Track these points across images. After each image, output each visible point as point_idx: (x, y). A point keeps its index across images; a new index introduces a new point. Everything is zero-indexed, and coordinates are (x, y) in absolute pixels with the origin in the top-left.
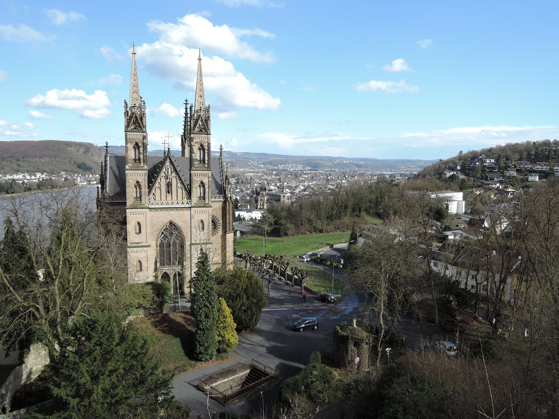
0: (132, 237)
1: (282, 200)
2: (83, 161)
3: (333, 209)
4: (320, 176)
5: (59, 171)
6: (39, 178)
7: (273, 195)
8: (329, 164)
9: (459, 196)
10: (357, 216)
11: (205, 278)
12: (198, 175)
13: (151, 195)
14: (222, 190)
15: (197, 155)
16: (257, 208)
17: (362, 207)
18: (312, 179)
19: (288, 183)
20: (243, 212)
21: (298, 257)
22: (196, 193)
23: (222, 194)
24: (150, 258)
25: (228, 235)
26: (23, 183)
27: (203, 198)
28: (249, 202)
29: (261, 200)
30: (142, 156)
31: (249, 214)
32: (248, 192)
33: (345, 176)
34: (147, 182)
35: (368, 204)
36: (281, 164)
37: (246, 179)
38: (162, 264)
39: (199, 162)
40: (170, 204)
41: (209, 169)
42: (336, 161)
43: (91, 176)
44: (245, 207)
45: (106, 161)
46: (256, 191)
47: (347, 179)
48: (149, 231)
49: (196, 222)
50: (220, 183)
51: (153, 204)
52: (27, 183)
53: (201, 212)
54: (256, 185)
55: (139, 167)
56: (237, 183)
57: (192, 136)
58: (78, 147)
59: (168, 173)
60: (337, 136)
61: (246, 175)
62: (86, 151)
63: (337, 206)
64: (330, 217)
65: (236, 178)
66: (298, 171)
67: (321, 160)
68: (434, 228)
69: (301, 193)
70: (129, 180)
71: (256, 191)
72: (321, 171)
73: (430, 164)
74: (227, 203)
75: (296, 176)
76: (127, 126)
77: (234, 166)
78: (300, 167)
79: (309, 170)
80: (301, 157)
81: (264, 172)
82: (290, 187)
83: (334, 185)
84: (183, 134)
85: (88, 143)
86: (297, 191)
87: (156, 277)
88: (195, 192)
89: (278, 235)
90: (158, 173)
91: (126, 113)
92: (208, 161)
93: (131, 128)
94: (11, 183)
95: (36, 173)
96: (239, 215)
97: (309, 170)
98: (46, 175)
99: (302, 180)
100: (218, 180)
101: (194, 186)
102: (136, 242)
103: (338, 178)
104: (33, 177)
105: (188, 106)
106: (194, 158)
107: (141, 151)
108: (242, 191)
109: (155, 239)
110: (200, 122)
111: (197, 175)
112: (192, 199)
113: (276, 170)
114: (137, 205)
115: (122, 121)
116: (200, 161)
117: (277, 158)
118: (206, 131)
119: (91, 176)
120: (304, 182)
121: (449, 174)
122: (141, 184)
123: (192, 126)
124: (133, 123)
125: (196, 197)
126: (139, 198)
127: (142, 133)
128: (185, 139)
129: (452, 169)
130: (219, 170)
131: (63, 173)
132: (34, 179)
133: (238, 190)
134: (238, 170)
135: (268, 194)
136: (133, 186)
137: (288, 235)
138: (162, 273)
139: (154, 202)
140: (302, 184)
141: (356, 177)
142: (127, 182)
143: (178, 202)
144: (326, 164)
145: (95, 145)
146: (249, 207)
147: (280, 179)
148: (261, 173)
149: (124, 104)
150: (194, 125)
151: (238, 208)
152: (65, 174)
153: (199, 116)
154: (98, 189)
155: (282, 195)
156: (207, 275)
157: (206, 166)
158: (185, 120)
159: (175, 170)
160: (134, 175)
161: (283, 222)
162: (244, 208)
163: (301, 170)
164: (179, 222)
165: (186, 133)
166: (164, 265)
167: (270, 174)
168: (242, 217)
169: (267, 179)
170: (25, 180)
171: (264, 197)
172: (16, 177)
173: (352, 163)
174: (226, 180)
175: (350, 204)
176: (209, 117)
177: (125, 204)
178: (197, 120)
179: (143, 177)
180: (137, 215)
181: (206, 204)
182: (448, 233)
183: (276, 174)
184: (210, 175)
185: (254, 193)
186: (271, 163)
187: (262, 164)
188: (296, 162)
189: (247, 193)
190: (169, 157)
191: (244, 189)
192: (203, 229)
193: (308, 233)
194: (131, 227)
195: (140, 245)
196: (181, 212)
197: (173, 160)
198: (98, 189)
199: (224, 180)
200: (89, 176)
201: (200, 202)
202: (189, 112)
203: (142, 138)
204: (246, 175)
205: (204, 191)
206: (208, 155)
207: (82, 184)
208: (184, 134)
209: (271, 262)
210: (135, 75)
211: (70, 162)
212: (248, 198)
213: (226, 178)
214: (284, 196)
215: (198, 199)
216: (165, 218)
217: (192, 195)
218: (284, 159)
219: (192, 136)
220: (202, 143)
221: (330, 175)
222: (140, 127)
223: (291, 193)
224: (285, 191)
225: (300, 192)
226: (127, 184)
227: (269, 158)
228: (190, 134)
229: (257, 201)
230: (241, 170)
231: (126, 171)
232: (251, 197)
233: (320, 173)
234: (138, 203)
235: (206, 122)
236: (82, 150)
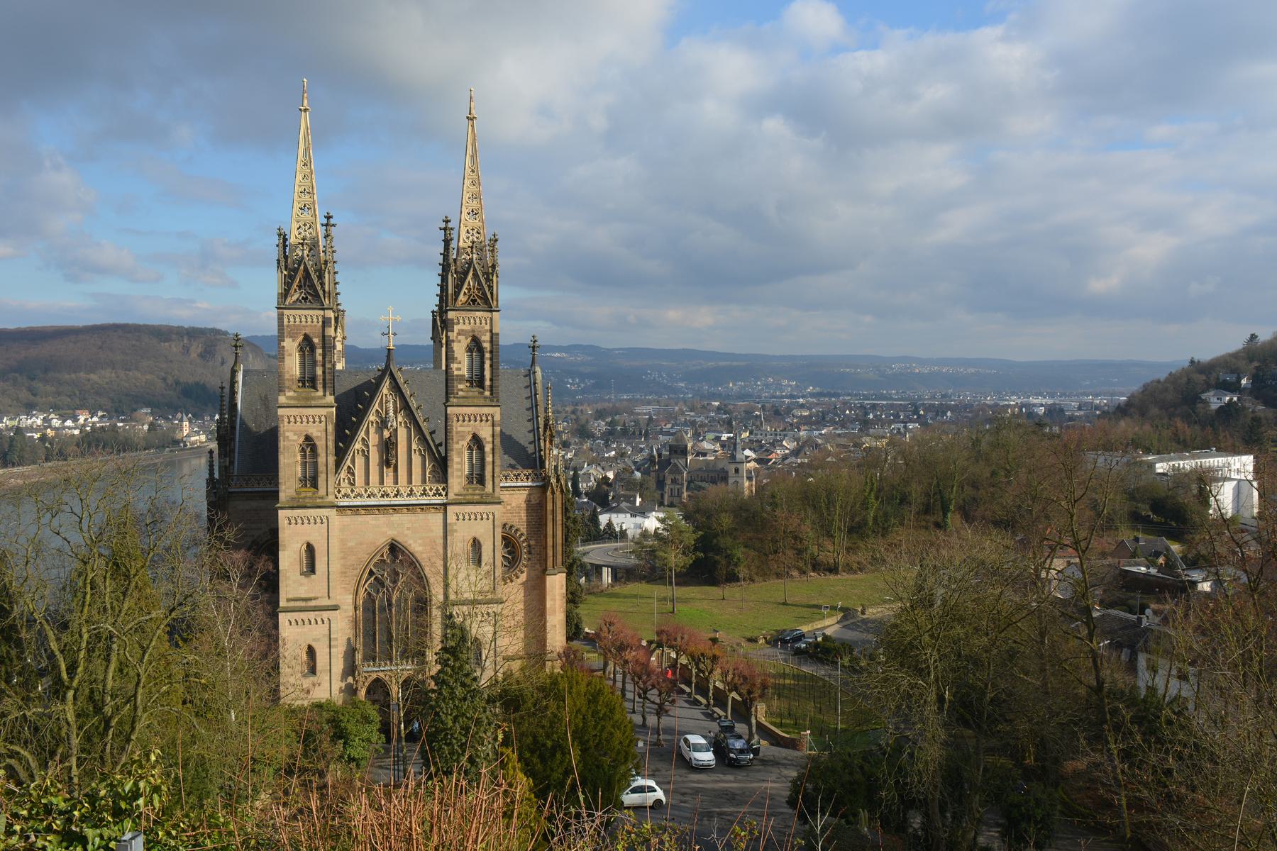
0: (292, 584)
1: (731, 481)
5: (135, 406)
6: (84, 426)
9: (1243, 464)
10: (938, 526)
11: (459, 692)
12: (466, 418)
13: (343, 474)
15: (462, 366)
19: (751, 433)
20: (621, 516)
21: (762, 641)
22: (459, 466)
24: (336, 639)
25: (549, 579)
26: (43, 438)
27: (477, 477)
28: (641, 487)
30: (319, 371)
31: (639, 520)
33: (916, 412)
34: (331, 438)
35: (968, 490)
37: (637, 422)
38: (370, 657)
39: (468, 384)
40: (392, 495)
41: (494, 400)
45: (233, 382)
48: (336, 567)
49: (459, 543)
51: (346, 495)
52: (53, 438)
53: (473, 517)
55: (314, 398)
57: (451, 315)
59: (387, 413)
63: (877, 498)
64: (857, 530)
65: (609, 420)
66: (782, 397)
68: (1161, 560)
69: (787, 461)
70: (287, 434)
73: (1162, 376)
74: (549, 493)
76: (284, 295)
78: (788, 385)
82: (751, 444)
83: (883, 437)
84: (436, 309)
87: (351, 691)
88: (458, 463)
89: (713, 582)
90: (362, 415)
91: (283, 260)
92: (491, 380)
93: (295, 298)
94: (12, 439)
95: (78, 412)
96: (610, 524)
97: (812, 395)
98: (103, 417)
99: (792, 425)
101: (456, 446)
102: (303, 596)
103: (897, 416)
104: (69, 423)
106: (456, 373)
107: (319, 358)
109: (352, 589)
111: (462, 418)
112: (450, 481)
114: (305, 498)
115: (272, 282)
116: (471, 381)
120: (799, 430)
121: (1216, 401)
122: (318, 443)
124: (300, 287)
125: (459, 477)
126: (311, 480)
127: (321, 312)
129: (1233, 387)
132: (70, 428)
136: (297, 448)
137: (738, 580)
138: (370, 680)
139: (349, 490)
141: (949, 414)
142: (281, 438)
143: (411, 490)
146: (639, 500)
147: (729, 423)
149: (276, 240)
152: (152, 414)
154: (211, 457)
156: (463, 685)
157: (487, 393)
159: (406, 407)
160: (298, 420)
161: (725, 542)
162: (624, 505)
164: (416, 546)
166: (374, 660)
168: (618, 529)
170: (49, 431)
172: (25, 421)
174: (545, 431)
175: (916, 491)
177: (275, 495)
179: (323, 424)
180: (306, 525)
181: (488, 495)
182: (1196, 575)
183: (719, 408)
187: (682, 380)
190: (391, 372)
192: (478, 562)
193: (795, 573)
194: (289, 558)
195: (313, 603)
196: (420, 517)
197: (401, 380)
198: (211, 457)
199: (541, 430)
201: (470, 491)
203: (321, 323)
206: (491, 366)
209: (673, 655)
210: (305, 165)
213: (546, 425)
214: (737, 471)
215: (465, 482)
216: (379, 530)
217: (450, 470)
220: (476, 334)
222: (317, 295)
224: (739, 457)
225: (785, 457)
226: (282, 444)
229: (661, 484)
231: (281, 412)
234: (308, 491)
236: (196, 348)
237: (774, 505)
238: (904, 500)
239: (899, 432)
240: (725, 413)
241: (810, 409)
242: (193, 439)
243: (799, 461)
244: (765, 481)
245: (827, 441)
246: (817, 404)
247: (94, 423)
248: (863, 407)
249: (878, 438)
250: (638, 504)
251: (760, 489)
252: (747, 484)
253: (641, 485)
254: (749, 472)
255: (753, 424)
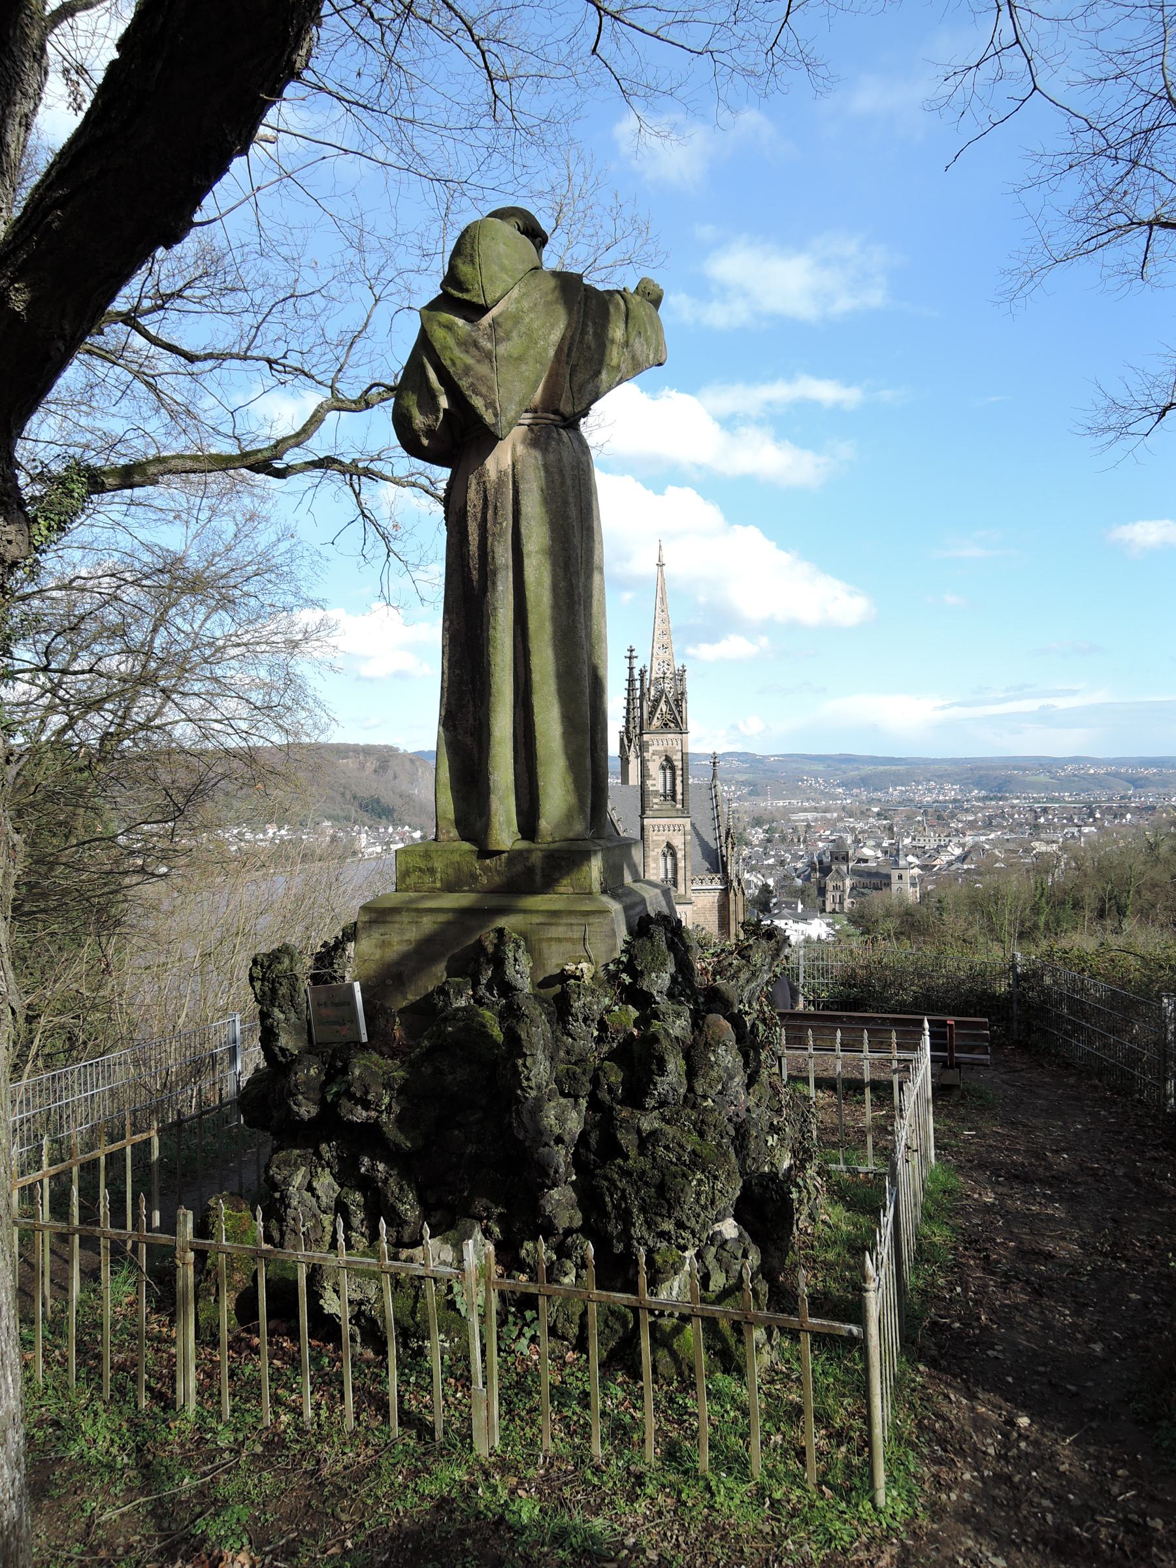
1: (894, 887)
2: (373, 793)
3: (1036, 910)
4: (1012, 816)
5: (317, 819)
7: (870, 874)
8: (1043, 778)
14: (717, 863)
15: (657, 782)
16: (823, 910)
17: (1127, 906)
18: (989, 825)
19: (914, 839)
23: (718, 872)
28: (802, 893)
29: (836, 888)
31: (801, 926)
32: (799, 865)
33: (1091, 814)
36: (895, 785)
37: (795, 829)
41: (685, 812)
42: (1065, 770)
43: (391, 830)
44: (790, 908)
46: (821, 862)
47: (1099, 823)
50: (713, 844)
54: (821, 845)
56: (769, 841)
58: (361, 757)
60: (1074, 692)
61: (794, 817)
62: (380, 767)
63: (1048, 903)
65: (766, 827)
66: (946, 801)
67: (1015, 769)
69: (953, 867)
71: (821, 862)
72: (1016, 802)
74: (732, 895)
75: (940, 817)
77: (758, 795)
78: (952, 792)
79: (978, 799)
80: (955, 761)
81: (844, 808)
84: (623, 729)
85: (386, 746)
86: (943, 859)
97: (978, 799)
99: (956, 830)
100: (709, 837)
101: (652, 853)
103: (1070, 819)
105: (636, 673)
106: (651, 788)
108: (782, 863)
110: (663, 706)
113: (879, 800)
117: (881, 768)
118: (677, 725)
119: (391, 830)
123: (645, 716)
128: (630, 741)
130: (710, 814)
131: (327, 823)
132: (261, 840)
133: (771, 861)
134: (771, 804)
135: (855, 872)
140: (955, 840)
141: (1129, 816)
144: (1034, 778)
145: (401, 751)
146: (800, 907)
147: (891, 828)
148: (835, 810)
150: (650, 713)
151: (769, 911)
153: (662, 692)
155: (895, 874)
157: (679, 806)
158: (629, 703)
162: (786, 911)
163: (955, 801)
165: (632, 726)
167: (862, 813)
169: (853, 829)
171: (843, 880)
173: (1117, 775)
174: (727, 839)
175: (1090, 896)
176: (682, 694)
178: (657, 701)
183: (878, 814)
184: (688, 827)
185: (814, 870)
186: (864, 782)
187: (838, 786)
188: (940, 777)
189: (796, 870)
191: (788, 857)
199: (723, 839)
200: (386, 829)
202: (638, 684)
204: (794, 817)
205: (675, 866)
207: (370, 850)
208: (627, 729)
211: (343, 794)
212: (799, 882)
213: (728, 833)
214: (900, 877)
218: (902, 768)
219: (646, 737)
221: (1045, 810)
223: (922, 867)
224: (902, 863)
225: (950, 863)
227: (858, 769)
228: (641, 734)
229: (822, 891)
230: (781, 803)
232: (807, 879)
233: (1013, 807)
235: (678, 705)
236: (371, 765)
237: (941, 909)
238: (1077, 905)
239: (1073, 836)
240: (886, 819)
241: (975, 814)
242: (370, 850)
243: (965, 867)
244: (930, 887)
245: (995, 847)
246: (983, 808)
247: (282, 836)
248: (1032, 810)
249: (1049, 842)
250: (799, 911)
251: (925, 896)
252: (911, 890)
253: (803, 892)
254: (913, 878)
255: (916, 830)
